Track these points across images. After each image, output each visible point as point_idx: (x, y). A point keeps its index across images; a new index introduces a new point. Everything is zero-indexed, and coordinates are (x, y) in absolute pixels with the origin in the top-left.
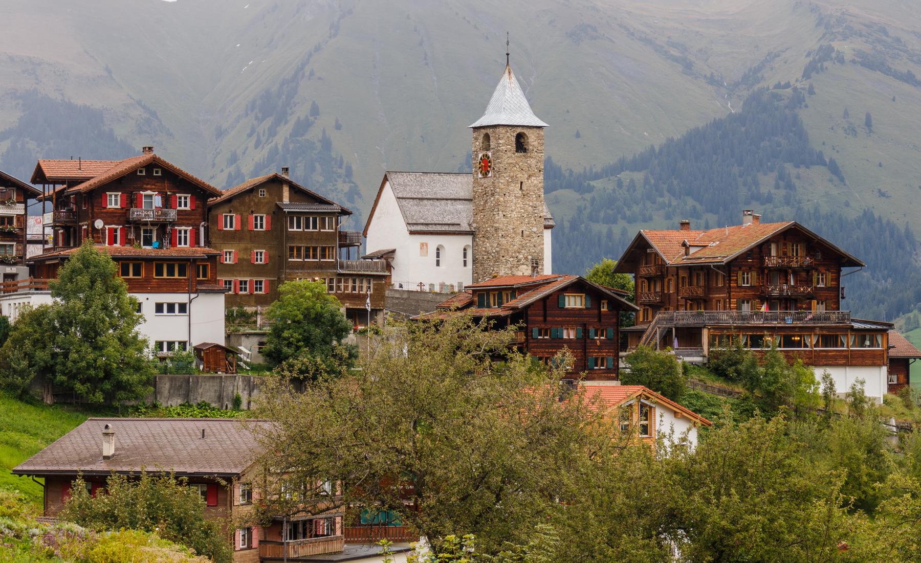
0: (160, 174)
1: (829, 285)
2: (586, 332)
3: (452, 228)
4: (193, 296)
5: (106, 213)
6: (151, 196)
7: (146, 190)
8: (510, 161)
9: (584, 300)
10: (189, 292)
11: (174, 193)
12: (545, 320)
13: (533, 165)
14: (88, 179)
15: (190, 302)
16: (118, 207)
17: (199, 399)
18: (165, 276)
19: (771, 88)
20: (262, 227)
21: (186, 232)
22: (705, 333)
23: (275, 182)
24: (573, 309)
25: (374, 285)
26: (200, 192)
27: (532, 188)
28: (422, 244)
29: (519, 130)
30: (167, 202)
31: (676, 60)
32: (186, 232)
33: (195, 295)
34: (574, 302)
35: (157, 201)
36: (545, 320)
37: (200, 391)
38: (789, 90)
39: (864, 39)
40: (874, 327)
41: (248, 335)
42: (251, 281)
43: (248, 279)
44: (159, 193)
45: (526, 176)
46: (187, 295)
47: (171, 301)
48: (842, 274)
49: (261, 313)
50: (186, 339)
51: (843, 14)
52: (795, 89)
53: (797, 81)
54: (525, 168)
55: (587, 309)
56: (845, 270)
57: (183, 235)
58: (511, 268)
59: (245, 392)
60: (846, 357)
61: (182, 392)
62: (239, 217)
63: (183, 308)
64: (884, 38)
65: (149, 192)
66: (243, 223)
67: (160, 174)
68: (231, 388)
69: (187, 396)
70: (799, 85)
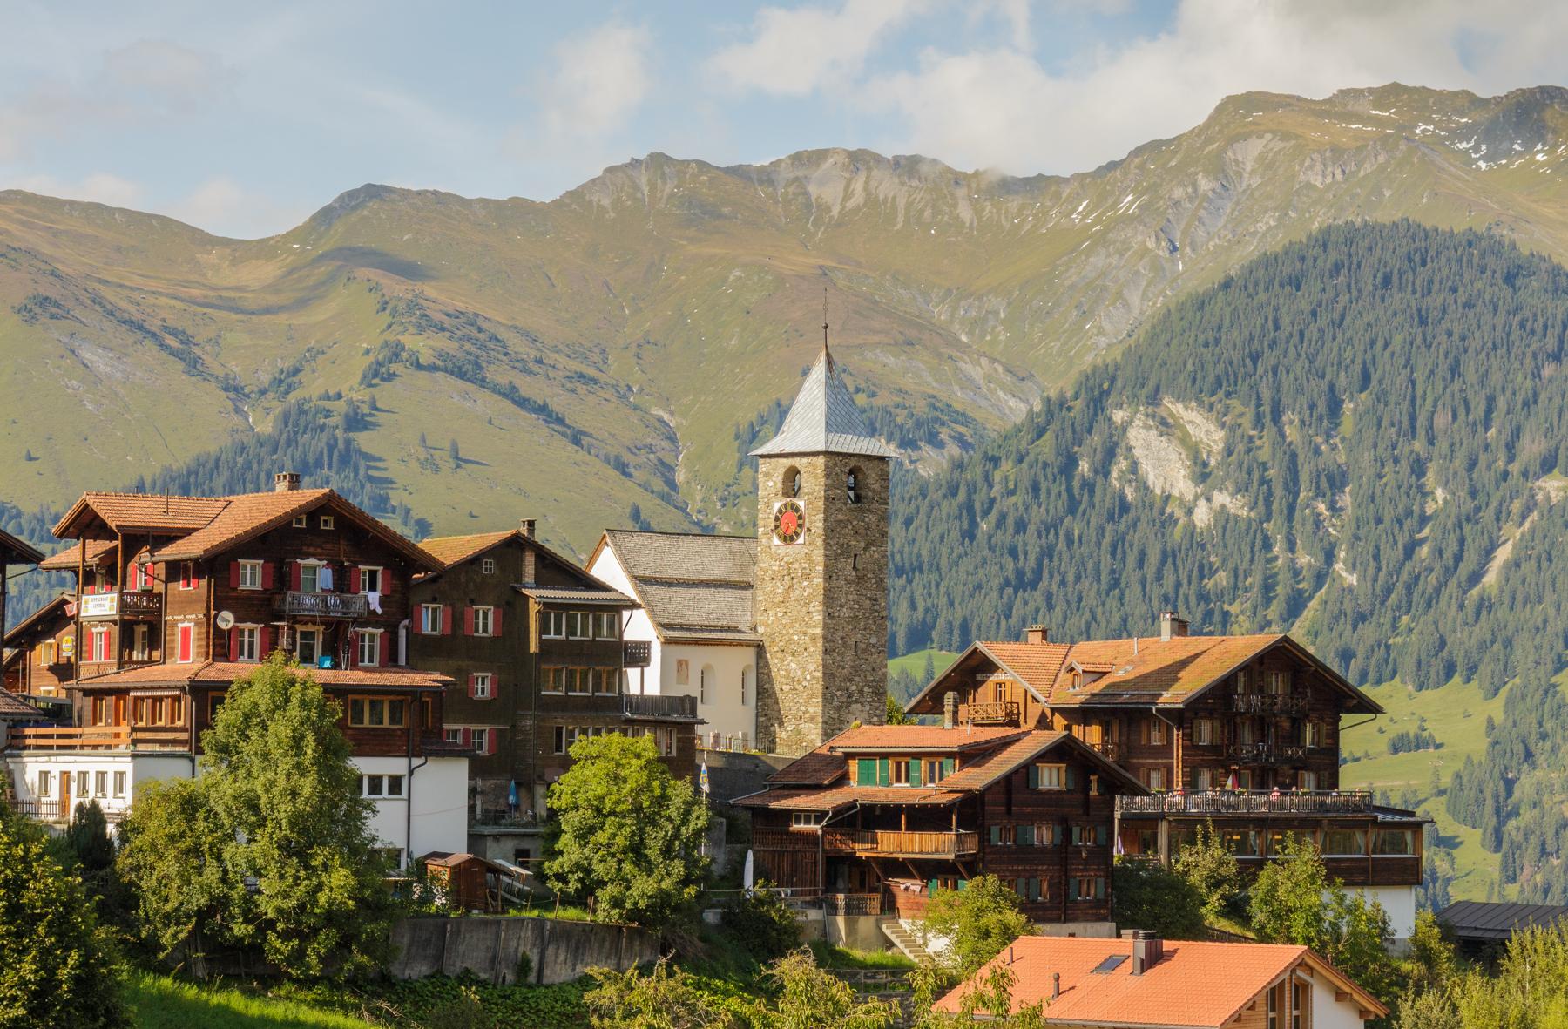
0: (331, 527)
1: (1323, 745)
2: (1067, 835)
3: (730, 636)
4: (416, 762)
5: (237, 598)
6: (314, 569)
7: (307, 556)
8: (840, 517)
9: (1063, 775)
10: (409, 755)
11: (355, 564)
12: (1009, 811)
13: (873, 526)
14: (188, 532)
15: (411, 773)
16: (258, 587)
17: (458, 964)
18: (367, 723)
19: (314, 397)
20: (485, 630)
21: (251, 632)
22: (1163, 828)
23: (516, 545)
24: (1049, 792)
25: (679, 740)
26: (400, 560)
27: (870, 567)
28: (680, 662)
29: (853, 462)
30: (343, 582)
31: (173, 353)
32: (251, 632)
33: (422, 760)
34: (1050, 778)
35: (325, 577)
36: (1009, 811)
37: (462, 948)
38: (341, 403)
39: (447, 334)
40: (1397, 818)
41: (497, 838)
42: (466, 731)
43: (460, 727)
44: (330, 562)
45: (863, 544)
46: (403, 762)
47: (376, 772)
48: (1341, 725)
49: (482, 793)
50: (400, 843)
51: (416, 296)
52: (350, 402)
53: (351, 389)
54: (862, 531)
55: (1069, 791)
56: (1346, 719)
57: (367, 643)
58: (838, 709)
59: (535, 950)
60: (1365, 871)
61: (431, 951)
62: (449, 609)
63: (396, 785)
64: (475, 333)
65: (312, 561)
66: (457, 620)
67: (331, 527)
68: (514, 944)
69: (439, 958)
70: (355, 395)
